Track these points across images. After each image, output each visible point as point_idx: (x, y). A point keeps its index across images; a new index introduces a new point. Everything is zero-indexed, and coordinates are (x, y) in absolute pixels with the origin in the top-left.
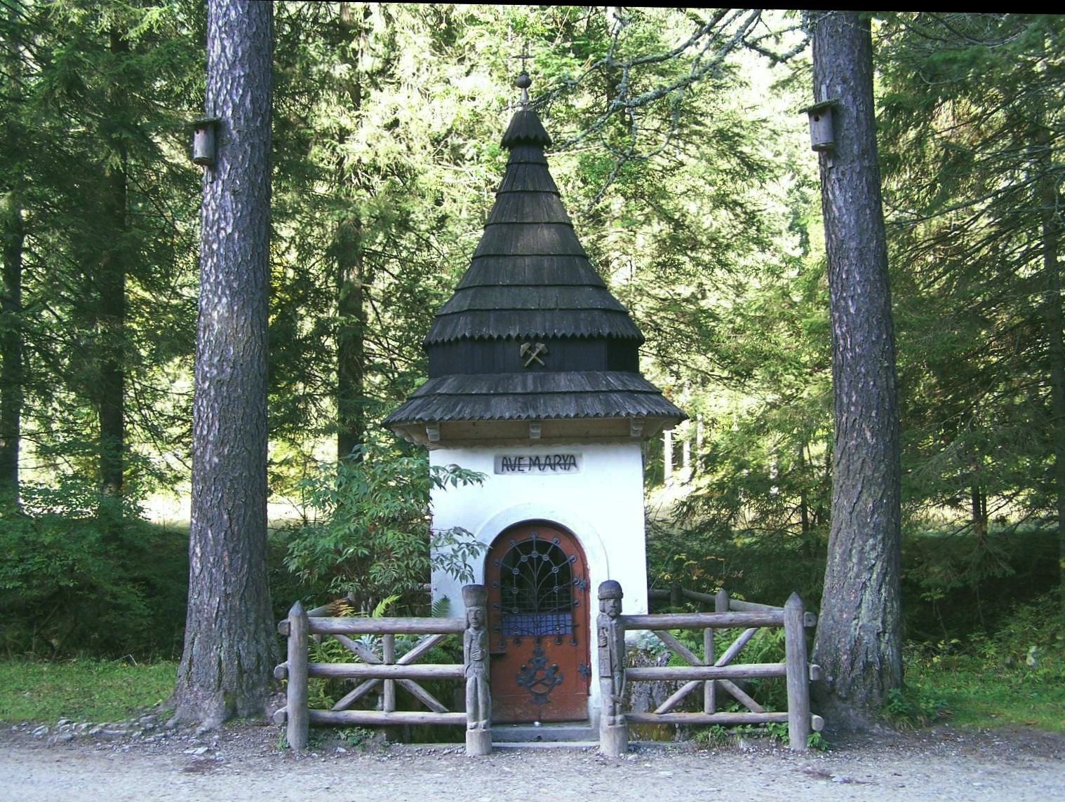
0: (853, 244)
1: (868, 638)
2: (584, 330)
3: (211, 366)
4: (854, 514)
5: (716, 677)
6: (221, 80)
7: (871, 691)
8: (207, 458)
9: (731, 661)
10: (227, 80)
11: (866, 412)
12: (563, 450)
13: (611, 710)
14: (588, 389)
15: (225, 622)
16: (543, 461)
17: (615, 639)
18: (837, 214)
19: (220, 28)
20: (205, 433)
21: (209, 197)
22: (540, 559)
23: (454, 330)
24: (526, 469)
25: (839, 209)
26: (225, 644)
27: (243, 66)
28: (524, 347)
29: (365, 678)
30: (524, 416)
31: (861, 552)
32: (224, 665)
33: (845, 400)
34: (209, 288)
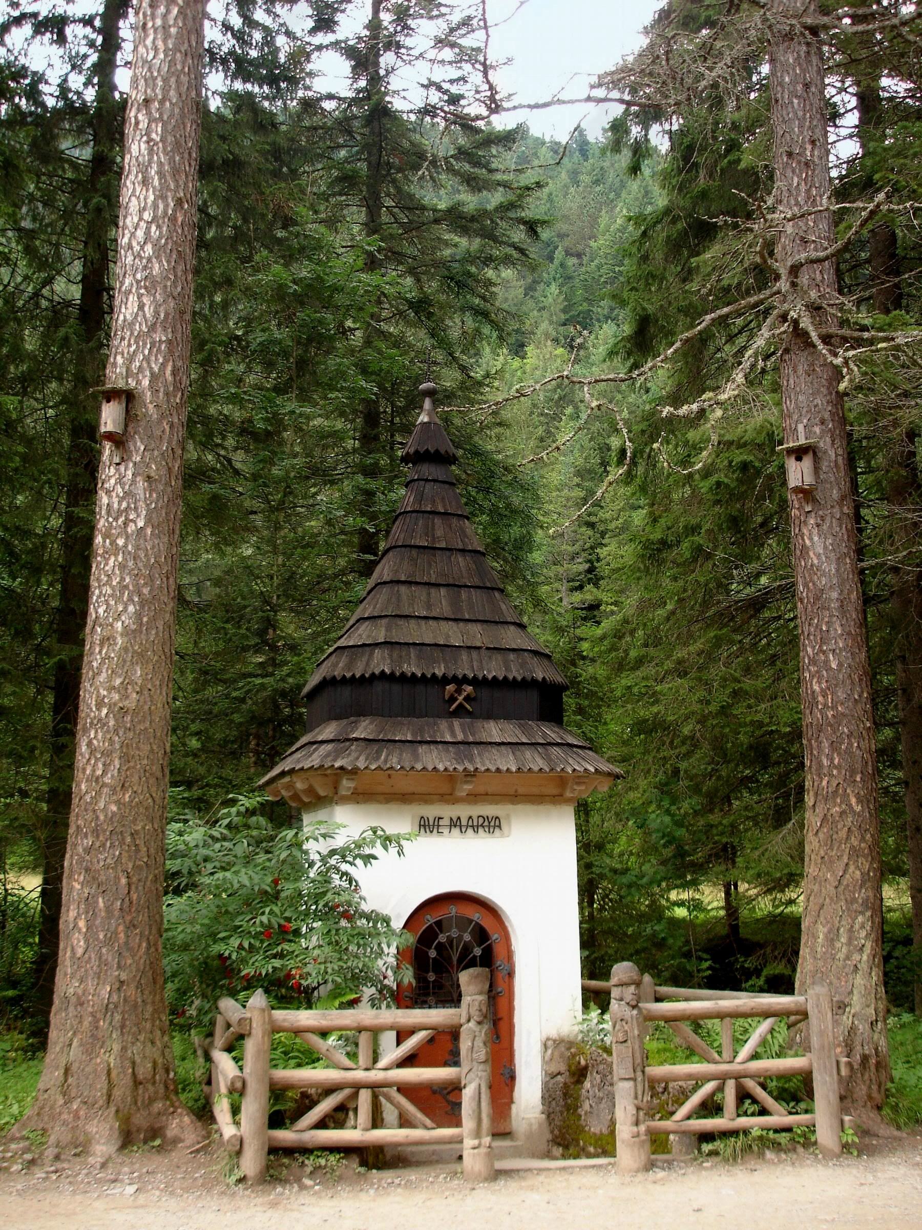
0: (835, 595)
1: (863, 1027)
2: (516, 673)
3: (111, 688)
4: (841, 888)
5: (738, 1077)
6: (137, 342)
7: (870, 1087)
8: (102, 805)
9: (755, 1056)
10: (145, 344)
11: (851, 776)
12: (489, 810)
13: (634, 1119)
14: (525, 740)
15: (118, 1017)
16: (464, 822)
17: (636, 1032)
18: (816, 561)
19: (138, 282)
20: (99, 772)
21: (113, 481)
22: (460, 938)
23: (368, 664)
24: (446, 831)
25: (818, 556)
26: (116, 1047)
27: (165, 329)
28: (450, 688)
29: (329, 1090)
30: (460, 768)
31: (851, 930)
32: (114, 1074)
33: (825, 762)
34: (109, 591)
